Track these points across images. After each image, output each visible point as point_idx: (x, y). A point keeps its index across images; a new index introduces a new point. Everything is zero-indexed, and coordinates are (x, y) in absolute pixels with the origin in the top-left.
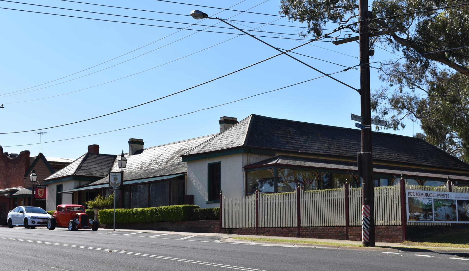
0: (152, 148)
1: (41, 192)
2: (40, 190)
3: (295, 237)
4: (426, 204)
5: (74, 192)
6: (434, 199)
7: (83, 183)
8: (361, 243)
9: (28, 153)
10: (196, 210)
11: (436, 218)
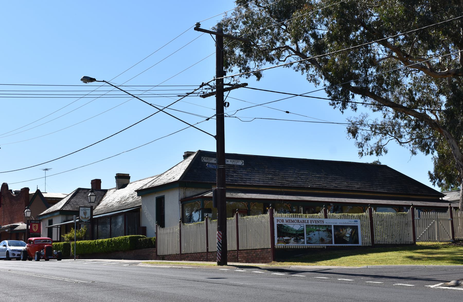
0: (134, 182)
3: (205, 261)
4: (297, 229)
5: (61, 225)
6: (306, 225)
7: (70, 217)
8: (216, 263)
9: (27, 190)
10: (141, 240)
11: (309, 241)
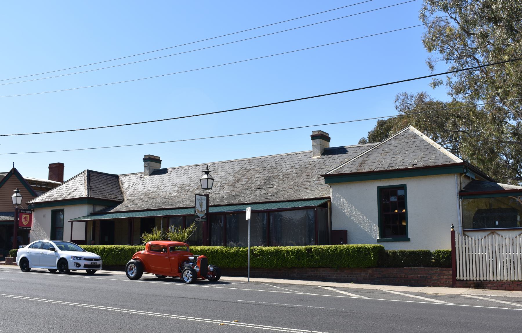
1: (25, 218)
2: (25, 215)
7: (98, 209)
